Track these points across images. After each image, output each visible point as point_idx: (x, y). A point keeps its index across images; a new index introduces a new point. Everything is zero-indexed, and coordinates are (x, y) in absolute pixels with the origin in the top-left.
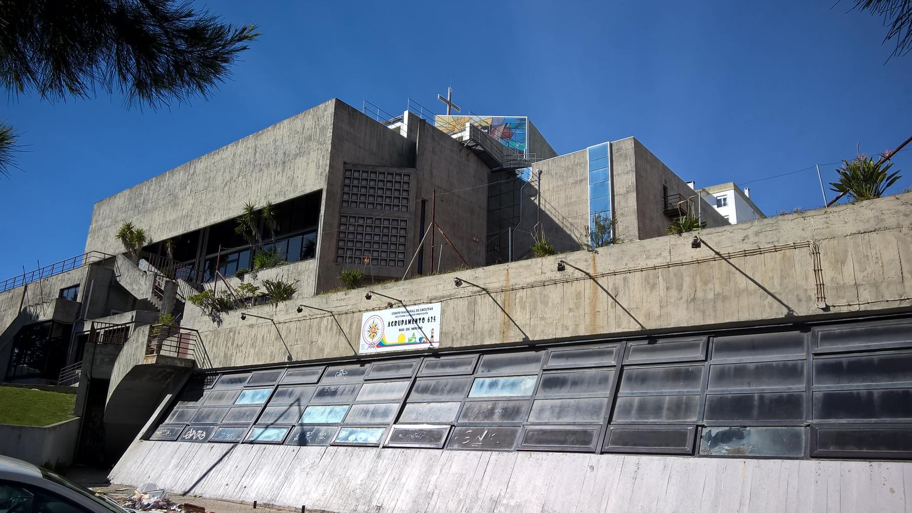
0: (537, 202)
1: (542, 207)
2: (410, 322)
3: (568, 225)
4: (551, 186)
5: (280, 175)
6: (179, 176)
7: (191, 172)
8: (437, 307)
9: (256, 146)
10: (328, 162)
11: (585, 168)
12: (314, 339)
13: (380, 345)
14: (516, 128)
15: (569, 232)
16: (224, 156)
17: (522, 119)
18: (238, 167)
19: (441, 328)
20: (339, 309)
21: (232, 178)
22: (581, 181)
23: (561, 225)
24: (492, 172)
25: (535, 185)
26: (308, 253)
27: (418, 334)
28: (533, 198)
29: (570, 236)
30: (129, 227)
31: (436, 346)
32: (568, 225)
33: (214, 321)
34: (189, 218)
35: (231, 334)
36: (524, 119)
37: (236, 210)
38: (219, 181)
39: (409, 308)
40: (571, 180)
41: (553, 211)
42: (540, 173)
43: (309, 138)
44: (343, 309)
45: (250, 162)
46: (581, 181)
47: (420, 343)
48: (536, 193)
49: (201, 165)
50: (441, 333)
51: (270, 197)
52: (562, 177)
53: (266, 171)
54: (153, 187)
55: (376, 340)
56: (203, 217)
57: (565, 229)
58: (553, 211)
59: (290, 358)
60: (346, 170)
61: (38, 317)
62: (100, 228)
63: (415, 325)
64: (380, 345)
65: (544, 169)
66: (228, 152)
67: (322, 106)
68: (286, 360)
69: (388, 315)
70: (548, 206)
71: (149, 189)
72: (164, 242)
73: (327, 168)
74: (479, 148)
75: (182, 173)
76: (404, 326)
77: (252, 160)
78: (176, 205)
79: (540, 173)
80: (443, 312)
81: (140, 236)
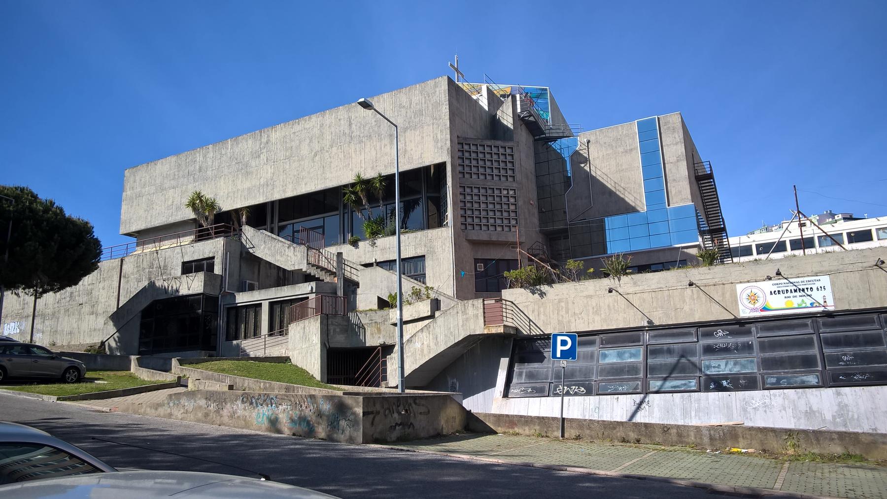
0: (587, 168)
1: (593, 173)
2: (795, 291)
3: (621, 189)
4: (601, 154)
5: (388, 147)
6: (246, 145)
7: (264, 140)
8: (825, 280)
9: (350, 119)
10: (448, 136)
11: (634, 139)
12: (678, 306)
13: (764, 309)
14: (538, 97)
15: (622, 196)
16: (307, 126)
17: (543, 90)
18: (329, 137)
19: (834, 295)
20: (705, 282)
21: (322, 149)
22: (631, 150)
23: (613, 189)
24: (535, 140)
25: (584, 153)
26: (440, 223)
27: (808, 301)
28: (582, 165)
29: (623, 200)
30: (199, 196)
31: (831, 309)
32: (621, 189)
33: (533, 293)
34: (270, 187)
35: (563, 304)
36: (546, 90)
37: (346, 178)
38: (305, 150)
39: (791, 280)
40: (621, 150)
41: (605, 177)
42: (589, 142)
43: (420, 113)
44: (712, 282)
45: (344, 134)
46: (631, 150)
47: (812, 307)
48: (586, 160)
49: (277, 134)
50: (834, 299)
51: (378, 168)
52: (610, 146)
53: (368, 143)
54: (211, 155)
55: (759, 305)
56: (290, 186)
57: (618, 193)
58: (605, 177)
59: (650, 322)
60: (461, 145)
61: (177, 291)
62: (140, 195)
63: (802, 293)
64: (764, 309)
65: (592, 139)
66: (313, 123)
67: (431, 83)
68: (646, 324)
69: (768, 286)
70: (599, 173)
71: (205, 156)
72: (237, 211)
73: (448, 143)
74: (531, 119)
75: (250, 142)
76: (789, 294)
77: (347, 131)
78: (248, 173)
79: (589, 142)
80: (833, 284)
81: (212, 206)
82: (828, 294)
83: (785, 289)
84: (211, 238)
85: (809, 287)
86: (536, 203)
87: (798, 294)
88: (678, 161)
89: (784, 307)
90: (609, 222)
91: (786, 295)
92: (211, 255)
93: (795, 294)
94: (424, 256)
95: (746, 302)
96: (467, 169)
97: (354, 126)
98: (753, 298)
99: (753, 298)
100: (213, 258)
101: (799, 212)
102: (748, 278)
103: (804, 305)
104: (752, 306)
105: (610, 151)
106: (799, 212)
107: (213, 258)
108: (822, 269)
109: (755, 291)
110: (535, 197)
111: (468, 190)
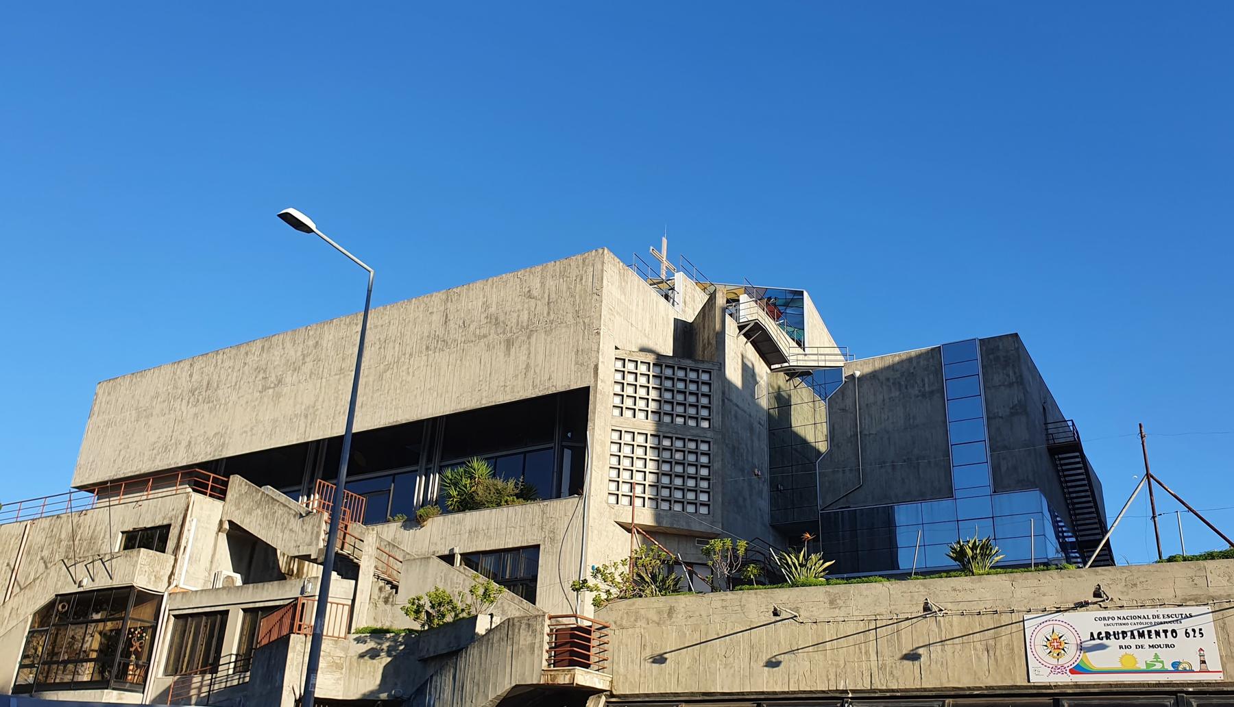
2: (1141, 635)
14: (786, 305)
47: (1177, 671)
82: (1211, 645)
83: (1120, 629)
84: (205, 494)
85: (1169, 627)
86: (767, 476)
87: (1146, 641)
88: (1012, 414)
89: (1118, 666)
90: (903, 514)
91: (1121, 642)
92: (165, 522)
93: (1139, 641)
94: (538, 546)
95: (1042, 652)
96: (629, 403)
97: (451, 325)
98: (1056, 645)
99: (1056, 645)
100: (169, 526)
101: (1148, 476)
102: (1050, 603)
103: (1158, 666)
104: (1054, 662)
105: (896, 394)
106: (1148, 476)
107: (169, 526)
108: (1195, 592)
109: (1060, 630)
110: (766, 465)
111: (627, 438)
